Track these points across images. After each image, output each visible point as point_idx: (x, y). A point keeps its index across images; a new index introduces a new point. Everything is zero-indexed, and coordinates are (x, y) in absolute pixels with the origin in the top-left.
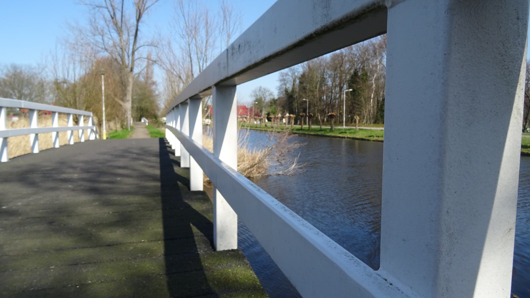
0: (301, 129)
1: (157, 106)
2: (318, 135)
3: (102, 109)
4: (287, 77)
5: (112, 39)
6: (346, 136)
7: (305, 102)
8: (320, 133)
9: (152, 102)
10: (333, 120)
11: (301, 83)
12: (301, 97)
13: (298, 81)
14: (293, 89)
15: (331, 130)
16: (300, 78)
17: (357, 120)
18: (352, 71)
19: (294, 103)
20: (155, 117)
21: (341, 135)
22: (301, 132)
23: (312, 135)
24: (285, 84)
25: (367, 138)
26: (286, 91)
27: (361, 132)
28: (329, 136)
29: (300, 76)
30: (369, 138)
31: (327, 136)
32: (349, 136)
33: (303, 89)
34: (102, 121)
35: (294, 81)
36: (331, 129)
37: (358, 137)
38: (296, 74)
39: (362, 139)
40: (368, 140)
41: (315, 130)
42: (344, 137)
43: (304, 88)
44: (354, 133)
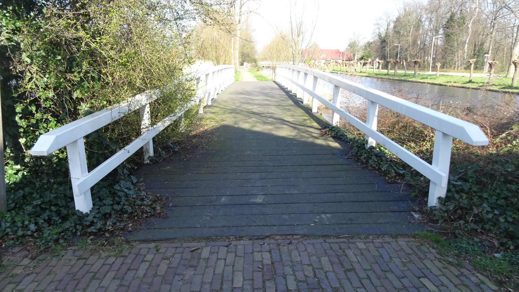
0: (388, 74)
1: (256, 52)
2: (401, 81)
3: (321, 146)
4: (382, 21)
5: (273, 244)
6: (426, 82)
7: (397, 47)
8: (403, 78)
9: (253, 48)
10: (417, 66)
11: (395, 27)
12: (393, 42)
13: (392, 25)
14: (386, 33)
15: (414, 76)
16: (395, 22)
17: (439, 67)
18: (448, 16)
19: (387, 48)
20: (255, 61)
21: (422, 81)
22: (386, 77)
23: (396, 80)
24: (379, 29)
25: (444, 84)
26: (380, 36)
27: (441, 78)
28: (411, 82)
29: (395, 20)
30: (446, 84)
31: (409, 81)
32: (429, 82)
33: (397, 32)
34: (400, 93)
35: (388, 25)
36: (415, 74)
37: (436, 82)
38: (391, 18)
39: (440, 85)
40: (445, 85)
41: (401, 76)
42: (425, 83)
43: (398, 32)
44: (435, 79)
